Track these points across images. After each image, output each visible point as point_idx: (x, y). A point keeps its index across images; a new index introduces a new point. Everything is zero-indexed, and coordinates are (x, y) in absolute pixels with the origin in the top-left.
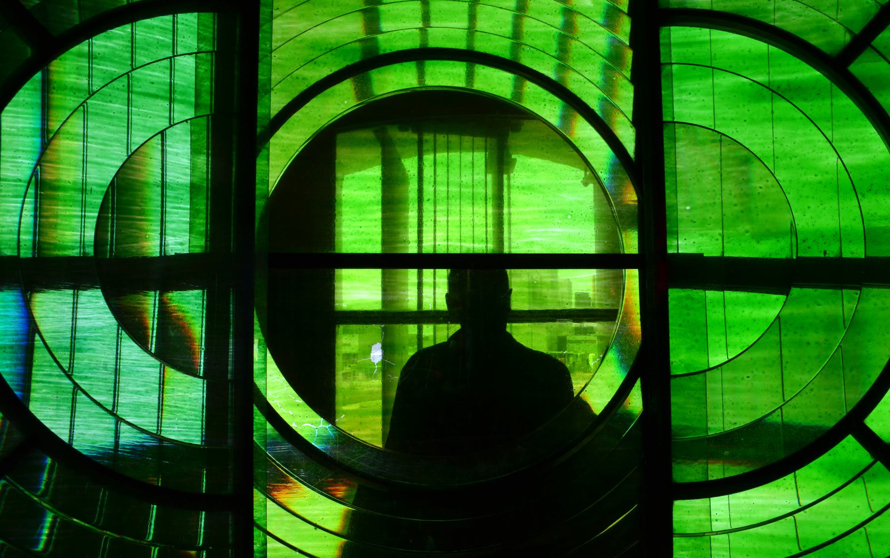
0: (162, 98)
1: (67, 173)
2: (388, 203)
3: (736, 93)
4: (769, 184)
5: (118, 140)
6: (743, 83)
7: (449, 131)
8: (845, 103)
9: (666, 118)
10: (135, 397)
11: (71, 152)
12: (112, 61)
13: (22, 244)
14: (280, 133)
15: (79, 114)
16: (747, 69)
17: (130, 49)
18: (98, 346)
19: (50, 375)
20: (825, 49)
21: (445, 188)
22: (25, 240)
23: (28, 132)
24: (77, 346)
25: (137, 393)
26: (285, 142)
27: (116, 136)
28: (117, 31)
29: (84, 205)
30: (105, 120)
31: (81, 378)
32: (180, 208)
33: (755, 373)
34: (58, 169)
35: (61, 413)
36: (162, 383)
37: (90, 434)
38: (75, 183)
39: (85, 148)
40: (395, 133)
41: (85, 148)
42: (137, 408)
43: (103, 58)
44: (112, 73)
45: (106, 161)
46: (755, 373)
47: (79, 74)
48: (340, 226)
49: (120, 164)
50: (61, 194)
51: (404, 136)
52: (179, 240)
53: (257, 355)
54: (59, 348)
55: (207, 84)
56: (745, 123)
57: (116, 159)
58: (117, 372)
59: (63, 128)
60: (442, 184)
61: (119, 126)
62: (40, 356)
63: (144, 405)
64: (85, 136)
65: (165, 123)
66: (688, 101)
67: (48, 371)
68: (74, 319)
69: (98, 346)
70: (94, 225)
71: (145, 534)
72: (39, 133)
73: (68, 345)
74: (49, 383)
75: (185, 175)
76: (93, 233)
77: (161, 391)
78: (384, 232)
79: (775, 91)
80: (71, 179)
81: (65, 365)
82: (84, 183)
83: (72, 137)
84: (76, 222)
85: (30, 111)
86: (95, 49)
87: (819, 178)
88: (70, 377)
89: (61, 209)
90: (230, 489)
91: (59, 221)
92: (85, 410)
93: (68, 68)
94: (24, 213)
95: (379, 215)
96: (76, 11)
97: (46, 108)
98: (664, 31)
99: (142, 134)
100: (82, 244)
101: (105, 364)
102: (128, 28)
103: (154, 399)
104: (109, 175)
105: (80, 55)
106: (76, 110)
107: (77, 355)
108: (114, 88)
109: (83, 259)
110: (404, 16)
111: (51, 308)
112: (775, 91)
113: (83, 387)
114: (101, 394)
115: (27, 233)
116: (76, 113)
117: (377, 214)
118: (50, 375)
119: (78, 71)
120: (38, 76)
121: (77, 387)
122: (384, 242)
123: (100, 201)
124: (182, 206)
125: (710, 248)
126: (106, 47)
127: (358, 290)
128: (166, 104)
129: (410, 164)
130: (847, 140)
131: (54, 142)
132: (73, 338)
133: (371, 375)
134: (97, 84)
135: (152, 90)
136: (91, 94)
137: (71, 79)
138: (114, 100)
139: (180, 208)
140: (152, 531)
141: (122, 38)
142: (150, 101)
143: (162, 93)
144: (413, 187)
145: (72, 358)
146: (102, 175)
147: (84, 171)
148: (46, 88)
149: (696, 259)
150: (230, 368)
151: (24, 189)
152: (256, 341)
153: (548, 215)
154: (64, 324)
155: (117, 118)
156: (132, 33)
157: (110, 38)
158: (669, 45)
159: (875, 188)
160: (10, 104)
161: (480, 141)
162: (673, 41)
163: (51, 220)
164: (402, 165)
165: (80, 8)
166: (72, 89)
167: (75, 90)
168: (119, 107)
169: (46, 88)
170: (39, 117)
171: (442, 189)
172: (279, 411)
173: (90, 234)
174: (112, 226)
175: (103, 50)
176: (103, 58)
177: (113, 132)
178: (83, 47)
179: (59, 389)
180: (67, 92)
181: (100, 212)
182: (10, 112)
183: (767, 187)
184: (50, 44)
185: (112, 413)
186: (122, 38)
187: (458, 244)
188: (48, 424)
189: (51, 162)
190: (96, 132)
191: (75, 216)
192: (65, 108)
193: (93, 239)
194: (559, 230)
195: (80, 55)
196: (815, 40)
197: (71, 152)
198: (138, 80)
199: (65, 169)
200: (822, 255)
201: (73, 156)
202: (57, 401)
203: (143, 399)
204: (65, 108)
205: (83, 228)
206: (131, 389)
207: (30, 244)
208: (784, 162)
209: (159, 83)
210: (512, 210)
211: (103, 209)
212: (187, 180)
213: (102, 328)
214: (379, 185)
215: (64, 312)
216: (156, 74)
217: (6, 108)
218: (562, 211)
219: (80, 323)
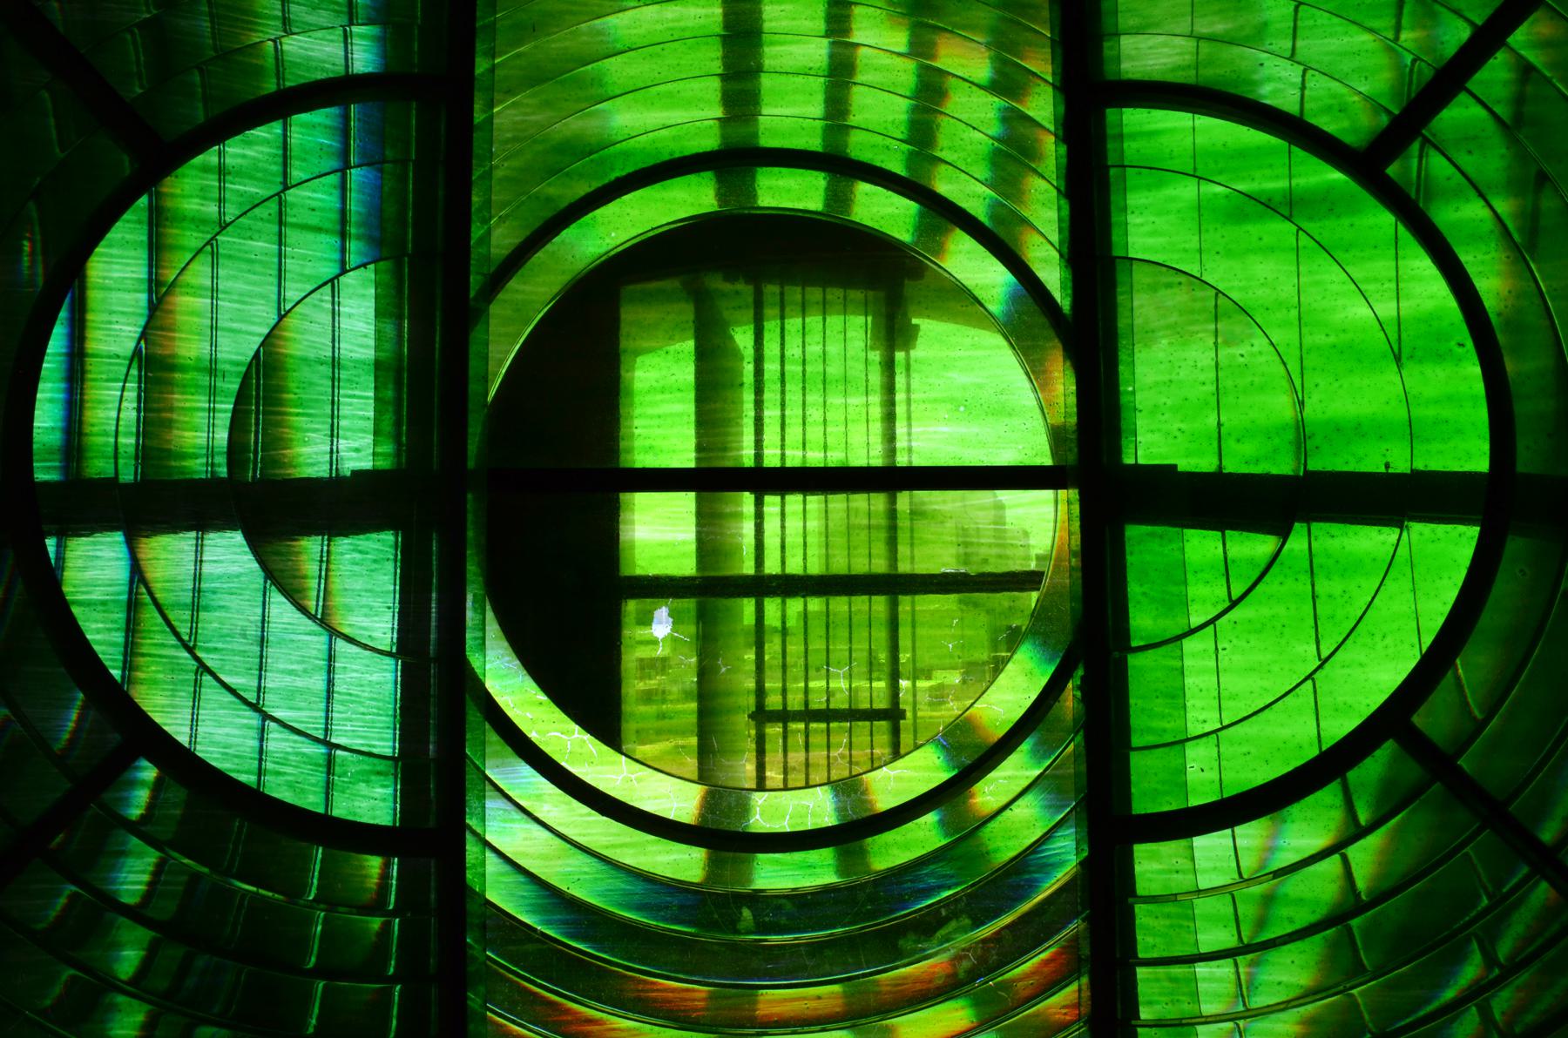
0: (327, 231)
1: (190, 347)
4: (1255, 349)
5: (262, 296)
6: (1215, 195)
7: (825, 283)
8: (1383, 220)
9: (1117, 252)
10: (288, 678)
11: (192, 313)
12: (251, 177)
13: (121, 450)
14: (513, 284)
15: (205, 258)
16: (1221, 172)
17: (280, 160)
18: (232, 602)
19: (163, 645)
20: (1349, 139)
22: (126, 445)
23: (129, 284)
24: (203, 602)
25: (291, 672)
26: (520, 297)
27: (257, 289)
28: (260, 132)
29: (213, 392)
30: (244, 266)
31: (208, 650)
32: (354, 396)
33: (1235, 641)
34: (173, 339)
35: (177, 701)
36: (331, 658)
37: (220, 738)
38: (198, 359)
39: (214, 309)
40: (716, 283)
41: (214, 309)
42: (290, 695)
43: (240, 173)
44: (252, 196)
45: (244, 327)
46: (1235, 641)
47: (205, 198)
49: (266, 331)
50: (177, 376)
51: (732, 292)
52: (356, 445)
53: (471, 616)
54: (178, 605)
56: (1217, 257)
57: (260, 324)
58: (262, 641)
59: (181, 278)
61: (264, 274)
62: (150, 616)
63: (301, 691)
64: (214, 291)
65: (333, 270)
66: (1148, 225)
67: (159, 638)
68: (199, 561)
69: (232, 602)
70: (228, 423)
71: (304, 888)
72: (145, 286)
73: (189, 600)
74: (160, 656)
75: (367, 347)
76: (225, 435)
77: (330, 670)
79: (1287, 207)
80: (193, 354)
81: (184, 630)
82: (213, 361)
83: (196, 291)
84: (200, 418)
85: (133, 253)
86: (229, 161)
87: (1332, 339)
88: (191, 650)
89: (178, 399)
90: (432, 823)
91: (175, 416)
92: (214, 697)
93: (190, 189)
94: (124, 404)
96: (200, 105)
97: (157, 249)
98: (1111, 114)
99: (299, 285)
100: (210, 451)
101: (244, 629)
102: (276, 128)
103: (319, 682)
104: (250, 345)
105: (206, 169)
106: (199, 251)
107: (203, 615)
108: (255, 218)
109: (213, 483)
111: (170, 554)
112: (1287, 207)
113: (209, 664)
114: (237, 674)
115: (127, 434)
116: (201, 257)
118: (163, 645)
119: (203, 193)
120: (143, 201)
121: (203, 668)
123: (236, 387)
124: (357, 393)
125: (1163, 450)
126: (244, 156)
127: (659, 533)
128: (334, 240)
129: (743, 338)
130: (1376, 280)
131: (170, 299)
132: (197, 591)
134: (231, 211)
135: (314, 220)
136: (223, 226)
137: (191, 205)
138: (256, 236)
139: (354, 396)
140: (315, 881)
141: (267, 142)
142: (310, 236)
143: (327, 225)
144: (749, 368)
145: (194, 620)
146: (238, 349)
147: (214, 343)
148: (158, 220)
149: (1164, 475)
150: (433, 636)
151: (124, 370)
152: (470, 597)
153: (929, 406)
154: (183, 570)
155: (261, 262)
156: (285, 136)
157: (249, 143)
158: (1121, 136)
159: (1419, 353)
160: (103, 243)
161: (856, 295)
162: (1126, 130)
164: (731, 338)
165: (205, 100)
166: (193, 220)
167: (199, 221)
168: (264, 246)
169: (158, 220)
170: (146, 262)
172: (512, 713)
173: (222, 436)
174: (257, 424)
175: (239, 161)
176: (240, 173)
177: (255, 284)
178: (210, 157)
179: (175, 667)
180: (185, 224)
181: (236, 404)
182: (102, 255)
183: (1252, 355)
184: (159, 156)
185: (255, 707)
186: (267, 142)
188: (157, 718)
189: (162, 329)
190: (230, 284)
191: (199, 409)
192: (182, 248)
193: (225, 443)
194: (945, 429)
195: (206, 169)
196: (1330, 125)
197: (192, 313)
198: (293, 205)
199: (298, 415)
200: (1383, 470)
201: (196, 319)
202: (174, 683)
203: (300, 683)
204: (182, 248)
205: (211, 427)
206: (282, 666)
207: (132, 450)
208: (1279, 315)
209: (323, 210)
211: (241, 398)
212: (369, 354)
213: (238, 576)
215: (182, 551)
216: (319, 196)
217: (98, 250)
218: (952, 400)
219: (206, 568)
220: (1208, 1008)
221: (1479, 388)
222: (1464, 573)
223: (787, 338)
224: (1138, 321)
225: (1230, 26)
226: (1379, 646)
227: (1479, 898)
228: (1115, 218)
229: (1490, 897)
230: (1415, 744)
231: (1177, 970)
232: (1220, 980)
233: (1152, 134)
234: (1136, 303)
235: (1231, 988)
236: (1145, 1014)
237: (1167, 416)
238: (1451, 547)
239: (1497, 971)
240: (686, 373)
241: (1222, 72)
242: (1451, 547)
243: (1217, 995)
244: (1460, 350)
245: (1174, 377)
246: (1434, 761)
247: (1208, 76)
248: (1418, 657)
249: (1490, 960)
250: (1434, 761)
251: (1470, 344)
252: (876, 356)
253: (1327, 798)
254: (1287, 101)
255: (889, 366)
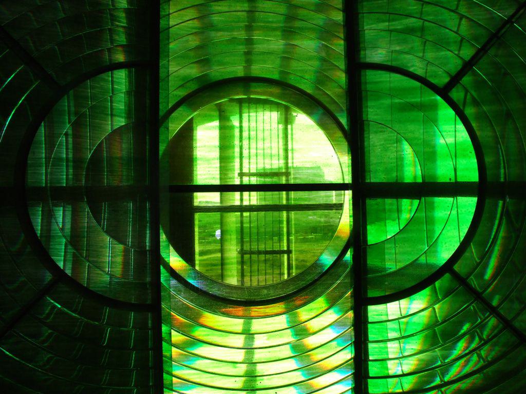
2: (223, 159)
3: (392, 107)
21: (255, 151)
33: (400, 244)
48: (196, 171)
55: (210, 205)
60: (253, 130)
78: (220, 173)
95: (218, 165)
110: (229, 63)
117: (217, 164)
122: (221, 179)
133: (319, 83)
163: (38, 171)
171: (253, 151)
187: (273, 162)
210: (294, 154)
214: (218, 150)
220: (391, 356)
221: (476, 166)
222: (470, 223)
223: (258, 141)
224: (371, 143)
225: (401, 48)
226: (444, 246)
227: (437, 362)
228: (364, 110)
229: (441, 362)
230: (455, 275)
231: (381, 345)
232: (395, 348)
233: (376, 83)
234: (371, 137)
235: (398, 351)
236: (371, 358)
237: (380, 174)
238: (469, 204)
239: (483, 342)
240: (216, 134)
241: (398, 63)
242: (469, 204)
243: (394, 353)
244: (470, 155)
245: (382, 161)
246: (460, 280)
247: (394, 64)
248: (459, 244)
249: (481, 339)
250: (460, 280)
251: (473, 152)
252: (281, 127)
253: (426, 292)
254: (420, 72)
255: (286, 129)
